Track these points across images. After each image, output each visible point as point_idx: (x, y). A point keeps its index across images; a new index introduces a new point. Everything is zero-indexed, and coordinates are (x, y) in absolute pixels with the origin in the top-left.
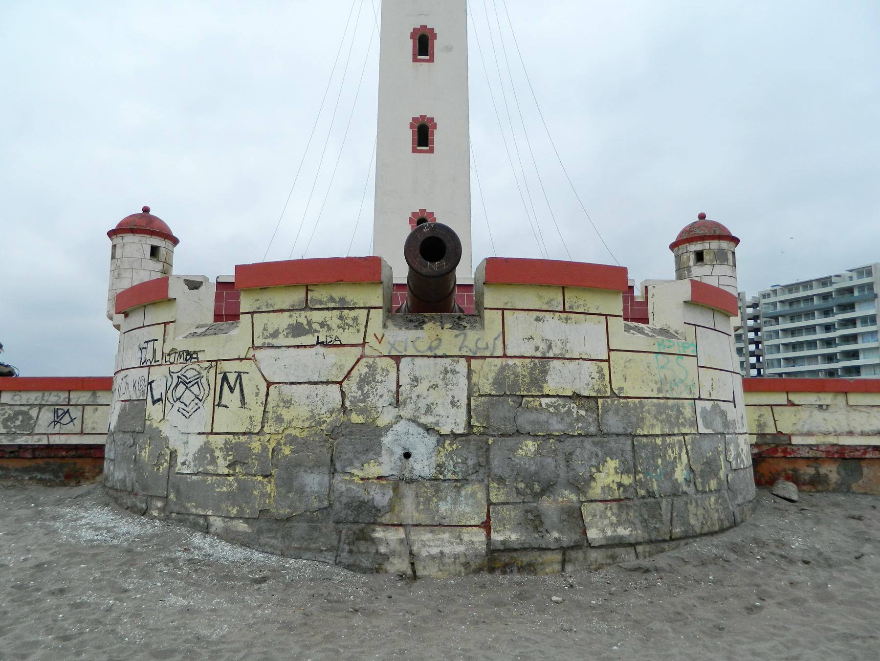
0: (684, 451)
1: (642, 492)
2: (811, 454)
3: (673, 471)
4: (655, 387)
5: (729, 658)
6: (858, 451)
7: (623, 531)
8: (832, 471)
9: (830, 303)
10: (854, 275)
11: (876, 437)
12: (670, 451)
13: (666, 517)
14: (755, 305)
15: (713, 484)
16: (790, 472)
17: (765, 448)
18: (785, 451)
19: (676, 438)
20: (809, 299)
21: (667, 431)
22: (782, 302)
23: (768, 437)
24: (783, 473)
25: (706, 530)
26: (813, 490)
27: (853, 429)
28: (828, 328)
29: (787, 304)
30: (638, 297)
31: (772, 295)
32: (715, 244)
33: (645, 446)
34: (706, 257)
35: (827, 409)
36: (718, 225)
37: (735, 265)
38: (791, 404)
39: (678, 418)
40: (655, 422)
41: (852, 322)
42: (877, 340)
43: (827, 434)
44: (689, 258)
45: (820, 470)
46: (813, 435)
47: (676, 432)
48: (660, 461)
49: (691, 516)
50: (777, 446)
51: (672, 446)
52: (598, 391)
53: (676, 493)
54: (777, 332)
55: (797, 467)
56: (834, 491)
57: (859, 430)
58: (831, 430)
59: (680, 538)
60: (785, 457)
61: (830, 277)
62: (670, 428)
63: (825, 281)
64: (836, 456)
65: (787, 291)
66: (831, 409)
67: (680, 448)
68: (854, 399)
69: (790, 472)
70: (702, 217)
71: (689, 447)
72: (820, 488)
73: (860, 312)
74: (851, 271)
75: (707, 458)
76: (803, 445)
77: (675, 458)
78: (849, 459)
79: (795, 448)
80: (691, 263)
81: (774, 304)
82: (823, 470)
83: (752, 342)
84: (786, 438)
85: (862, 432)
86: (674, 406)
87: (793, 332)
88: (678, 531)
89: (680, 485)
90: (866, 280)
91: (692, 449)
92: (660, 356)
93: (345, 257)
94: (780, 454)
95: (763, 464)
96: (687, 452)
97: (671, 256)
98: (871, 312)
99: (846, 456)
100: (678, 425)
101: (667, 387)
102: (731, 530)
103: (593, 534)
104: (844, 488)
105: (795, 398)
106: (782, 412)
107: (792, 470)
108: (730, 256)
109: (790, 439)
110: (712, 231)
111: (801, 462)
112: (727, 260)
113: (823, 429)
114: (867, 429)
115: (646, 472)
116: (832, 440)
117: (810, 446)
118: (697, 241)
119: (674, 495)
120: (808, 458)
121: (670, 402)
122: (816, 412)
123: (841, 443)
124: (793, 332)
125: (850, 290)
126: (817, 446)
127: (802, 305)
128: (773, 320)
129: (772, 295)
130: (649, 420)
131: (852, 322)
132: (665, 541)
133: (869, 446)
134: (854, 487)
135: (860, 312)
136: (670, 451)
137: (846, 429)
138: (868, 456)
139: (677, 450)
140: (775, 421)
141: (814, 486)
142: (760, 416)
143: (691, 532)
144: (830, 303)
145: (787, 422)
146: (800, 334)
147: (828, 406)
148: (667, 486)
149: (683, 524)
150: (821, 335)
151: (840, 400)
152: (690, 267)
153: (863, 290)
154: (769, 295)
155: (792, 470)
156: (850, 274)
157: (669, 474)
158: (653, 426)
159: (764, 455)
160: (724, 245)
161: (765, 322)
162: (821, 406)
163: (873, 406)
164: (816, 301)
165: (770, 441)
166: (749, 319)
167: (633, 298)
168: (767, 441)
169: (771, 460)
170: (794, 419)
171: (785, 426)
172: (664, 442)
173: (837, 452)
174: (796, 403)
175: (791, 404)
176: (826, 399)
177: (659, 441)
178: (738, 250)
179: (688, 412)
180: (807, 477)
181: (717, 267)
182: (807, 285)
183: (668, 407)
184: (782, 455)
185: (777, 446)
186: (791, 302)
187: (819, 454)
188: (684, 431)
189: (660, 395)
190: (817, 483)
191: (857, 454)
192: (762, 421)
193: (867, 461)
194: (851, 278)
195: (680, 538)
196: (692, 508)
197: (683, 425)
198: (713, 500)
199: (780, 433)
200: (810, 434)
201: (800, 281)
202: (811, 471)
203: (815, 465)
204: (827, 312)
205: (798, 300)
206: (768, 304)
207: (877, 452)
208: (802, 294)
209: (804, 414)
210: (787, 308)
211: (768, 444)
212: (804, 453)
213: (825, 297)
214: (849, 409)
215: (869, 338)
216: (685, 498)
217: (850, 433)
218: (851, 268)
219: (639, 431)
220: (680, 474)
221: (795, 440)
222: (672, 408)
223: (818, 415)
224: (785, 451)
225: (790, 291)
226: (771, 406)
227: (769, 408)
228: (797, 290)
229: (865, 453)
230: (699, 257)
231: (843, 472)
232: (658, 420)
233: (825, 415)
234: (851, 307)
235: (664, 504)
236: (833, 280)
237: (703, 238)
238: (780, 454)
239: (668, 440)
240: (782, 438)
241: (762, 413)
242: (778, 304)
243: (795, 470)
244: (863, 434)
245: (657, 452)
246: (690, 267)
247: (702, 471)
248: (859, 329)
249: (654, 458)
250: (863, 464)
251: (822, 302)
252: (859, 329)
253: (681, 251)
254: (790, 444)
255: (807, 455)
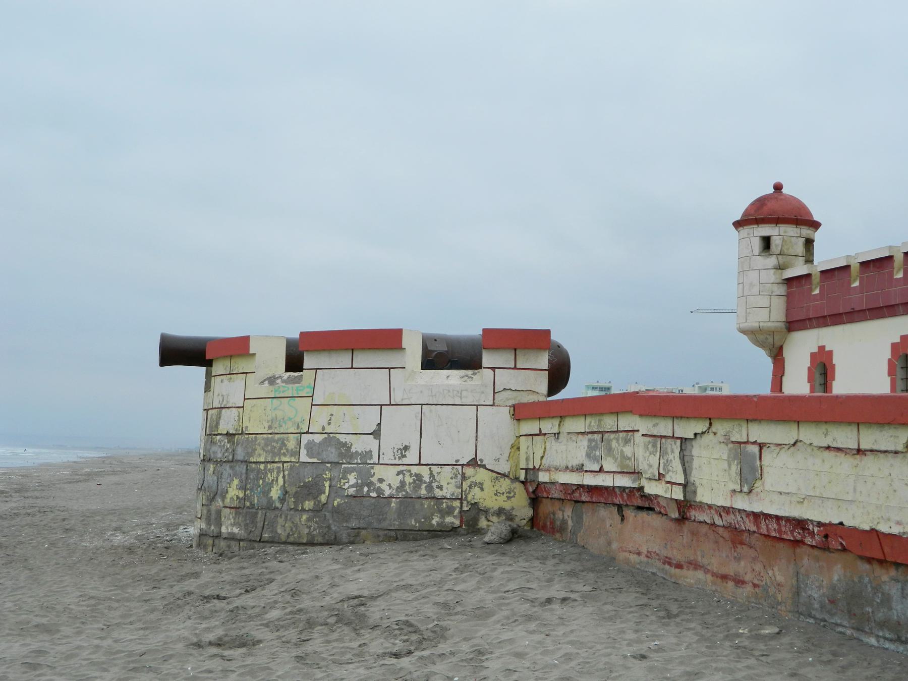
0: (281, 475)
1: (248, 504)
3: (270, 491)
4: (267, 425)
5: (2, 492)
7: (236, 530)
12: (269, 475)
13: (260, 525)
15: (308, 505)
19: (275, 465)
21: (269, 459)
25: (291, 539)
33: (253, 470)
39: (281, 448)
40: (261, 452)
47: (277, 460)
48: (261, 482)
49: (279, 527)
51: (271, 471)
52: (236, 430)
53: (270, 507)
59: (267, 542)
62: (272, 457)
67: (278, 473)
70: (778, 188)
71: (286, 473)
75: (305, 483)
77: (273, 480)
86: (279, 439)
88: (266, 535)
89: (274, 502)
91: (289, 475)
92: (275, 400)
93: (834, 362)
96: (284, 477)
100: (279, 454)
101: (276, 425)
102: (326, 549)
103: (224, 530)
115: (251, 490)
119: (268, 508)
121: (277, 436)
130: (259, 450)
132: (255, 541)
136: (269, 475)
139: (275, 474)
143: (276, 539)
148: (264, 501)
149: (272, 532)
157: (266, 493)
158: (260, 455)
172: (266, 467)
177: (262, 467)
179: (291, 444)
183: (274, 441)
188: (284, 459)
189: (270, 431)
195: (267, 542)
196: (281, 521)
197: (284, 455)
198: (304, 517)
216: (277, 512)
219: (252, 460)
220: (275, 493)
222: (277, 442)
232: (264, 450)
235: (260, 514)
237: (777, 221)
239: (269, 466)
245: (261, 475)
247: (296, 493)
249: (258, 479)
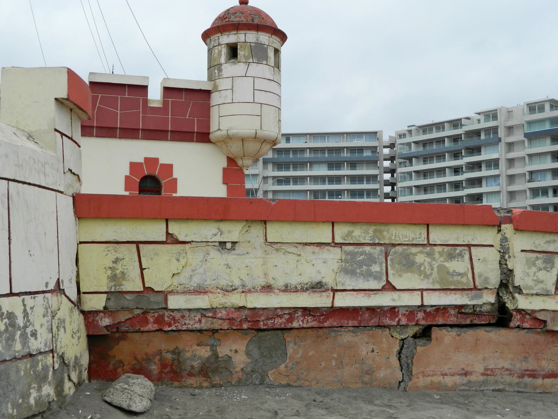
2: (205, 324)
6: (280, 316)
8: (237, 352)
9: (460, 145)
10: (482, 118)
11: (306, 295)
14: (392, 146)
16: (169, 356)
17: (123, 317)
18: (159, 320)
20: (440, 141)
22: (416, 143)
23: (128, 297)
24: (158, 358)
26: (205, 384)
27: (272, 282)
28: (457, 170)
29: (421, 145)
30: (153, 101)
31: (408, 135)
32: (251, 37)
34: (241, 53)
35: (233, 249)
36: (258, 12)
37: (277, 65)
38: (171, 239)
41: (477, 166)
42: (499, 185)
43: (229, 290)
44: (220, 52)
45: (219, 349)
46: (206, 292)
50: (145, 313)
54: (410, 173)
55: (181, 346)
56: (240, 383)
57: (281, 283)
58: (237, 283)
60: (160, 330)
61: (460, 120)
63: (456, 123)
64: (245, 326)
65: (421, 131)
66: (239, 249)
68: (278, 232)
69: (169, 356)
72: (217, 380)
73: (485, 155)
74: (479, 114)
76: (190, 310)
78: (264, 329)
79: (177, 315)
80: (223, 60)
81: (409, 144)
82: (223, 351)
83: (387, 183)
84: (160, 298)
85: (286, 286)
87: (425, 174)
90: (492, 124)
94: (151, 326)
95: (122, 343)
97: (204, 48)
98: (495, 156)
99: (261, 325)
104: (254, 379)
105: (176, 229)
106: (156, 254)
107: (173, 352)
108: (271, 54)
109: (166, 300)
110: (250, 19)
111: (186, 337)
112: (267, 58)
113: (223, 283)
114: (294, 281)
116: (237, 300)
117: (202, 312)
118: (230, 30)
120: (200, 331)
122: (214, 254)
123: (249, 305)
124: (425, 174)
125: (477, 133)
126: (213, 310)
127: (435, 147)
128: (408, 161)
129: (408, 135)
131: (477, 166)
133: (296, 309)
134: (271, 377)
135: (485, 155)
137: (262, 282)
138: (295, 324)
140: (142, 269)
141: (206, 376)
142: (116, 261)
144: (460, 145)
145: (162, 270)
146: (432, 176)
147: (234, 243)
150: (450, 178)
151: (256, 231)
152: (221, 65)
153: (490, 134)
154: (404, 135)
155: (173, 352)
156: (478, 117)
159: (124, 328)
160: (264, 38)
161: (400, 163)
162: (223, 244)
163: (306, 244)
164: (447, 144)
165: (132, 305)
166: (385, 160)
167: (146, 101)
168: (126, 304)
169: (137, 336)
170: (175, 267)
171: (157, 280)
173: (246, 319)
174: (181, 239)
175: (171, 239)
176: (232, 231)
178: (285, 49)
180: (196, 364)
181: (253, 67)
182: (439, 126)
184: (156, 327)
185: (145, 313)
186: (425, 143)
187: (217, 325)
190: (212, 371)
191: (279, 322)
192: (120, 268)
193: (295, 332)
194: (479, 121)
199: (151, 289)
200: (200, 291)
201: (434, 122)
202: (204, 352)
203: (212, 341)
204: (456, 155)
205: (430, 142)
206: (403, 144)
207: (309, 319)
208: (435, 135)
209: (194, 257)
210: (421, 149)
211: (129, 310)
212: (192, 323)
213: (455, 139)
214: (268, 248)
215: (492, 181)
217: (268, 288)
218: (479, 111)
221: (174, 302)
223: (217, 259)
224: (159, 320)
225: (424, 132)
226: (137, 243)
227: (134, 246)
228: (431, 131)
229: (290, 320)
230: (233, 52)
231: (256, 353)
233: (230, 258)
234: (476, 150)
236: (463, 122)
237: (237, 27)
238: (151, 326)
240: (153, 298)
241: (120, 256)
242: (413, 144)
243: (177, 352)
244: (287, 289)
246: (221, 65)
248: (484, 173)
250: (289, 337)
251: (452, 144)
252: (484, 173)
253: (212, 43)
254: (166, 309)
255: (197, 326)
